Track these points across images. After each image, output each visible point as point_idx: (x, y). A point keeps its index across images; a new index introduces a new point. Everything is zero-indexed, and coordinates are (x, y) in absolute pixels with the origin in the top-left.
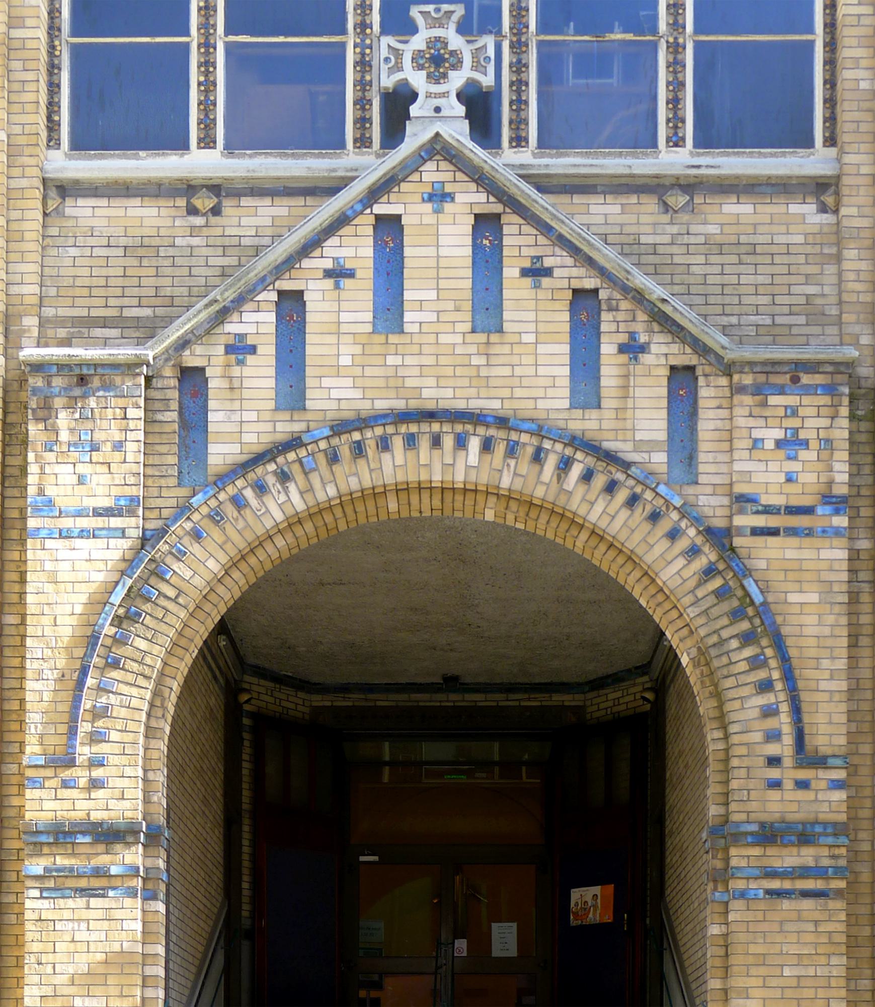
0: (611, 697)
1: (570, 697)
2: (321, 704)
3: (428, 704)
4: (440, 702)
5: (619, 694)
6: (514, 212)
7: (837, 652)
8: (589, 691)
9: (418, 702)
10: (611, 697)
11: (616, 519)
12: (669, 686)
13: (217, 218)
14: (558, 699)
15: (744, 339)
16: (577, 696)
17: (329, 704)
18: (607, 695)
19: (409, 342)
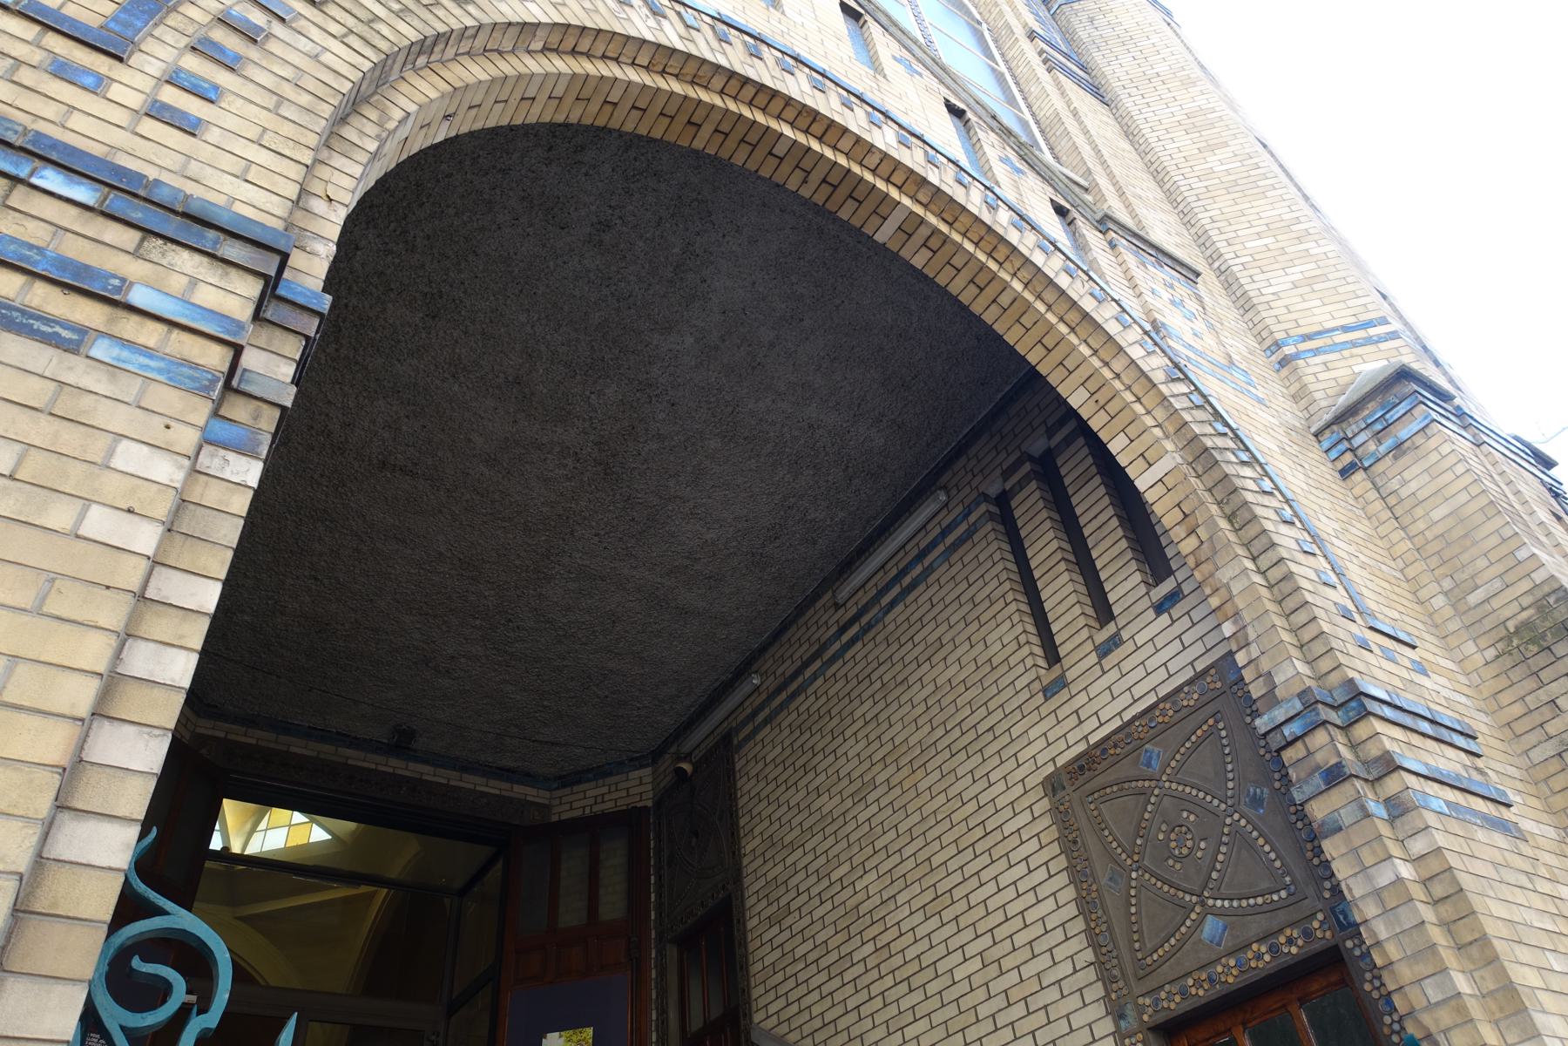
0: (589, 793)
1: (534, 792)
2: (210, 732)
3: (360, 764)
4: (377, 764)
5: (605, 790)
6: (1082, 574)
7: (1160, 489)
8: (557, 788)
9: (348, 758)
10: (589, 793)
11: (949, 608)
12: (740, 746)
13: (1028, 41)
14: (520, 791)
15: (693, 130)
16: (542, 792)
17: (222, 735)
18: (585, 792)
19: (1528, 699)
